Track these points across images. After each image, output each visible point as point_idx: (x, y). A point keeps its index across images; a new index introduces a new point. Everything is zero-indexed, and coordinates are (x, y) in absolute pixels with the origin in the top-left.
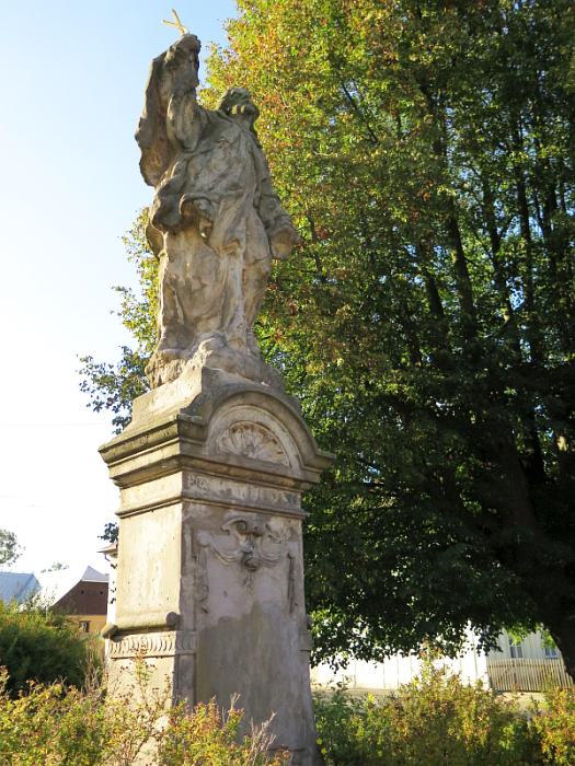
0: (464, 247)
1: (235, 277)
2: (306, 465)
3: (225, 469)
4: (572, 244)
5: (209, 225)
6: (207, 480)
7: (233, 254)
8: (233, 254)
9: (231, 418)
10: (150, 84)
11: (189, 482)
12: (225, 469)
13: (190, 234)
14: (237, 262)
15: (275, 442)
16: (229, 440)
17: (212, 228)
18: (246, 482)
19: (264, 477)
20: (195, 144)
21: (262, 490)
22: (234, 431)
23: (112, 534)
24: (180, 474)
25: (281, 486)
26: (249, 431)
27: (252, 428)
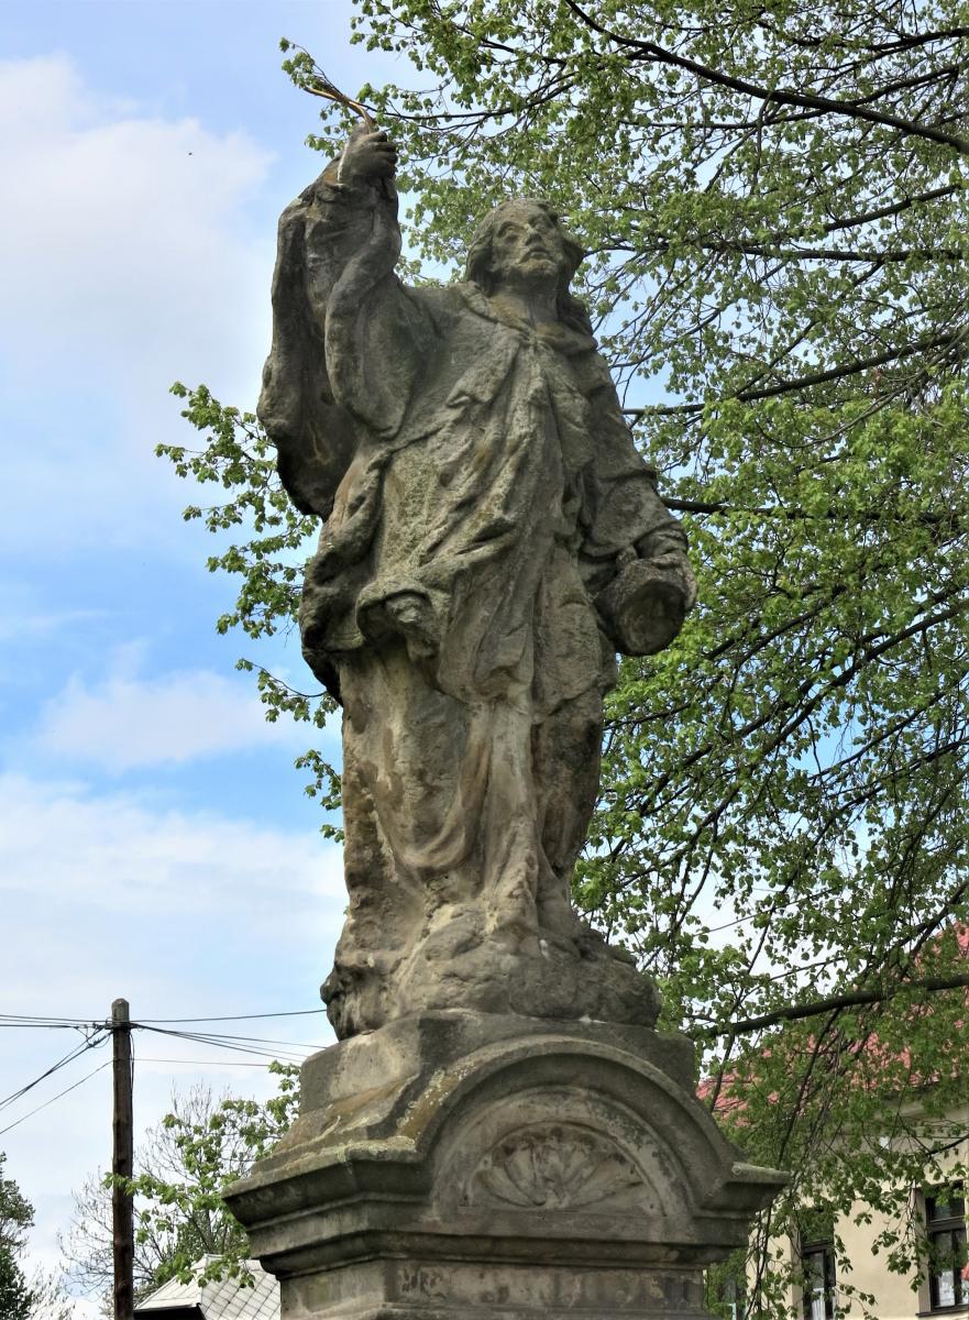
0: (825, 988)
1: (510, 760)
2: (703, 1208)
3: (487, 1245)
4: (967, 1003)
5: (427, 652)
6: (446, 1272)
7: (502, 698)
8: (502, 698)
9: (492, 1129)
10: (279, 283)
11: (402, 1282)
12: (487, 1245)
13: (395, 664)
14: (513, 717)
15: (622, 1160)
16: (499, 1174)
17: (433, 657)
18: (545, 1266)
19: (590, 1250)
20: (400, 412)
21: (591, 1277)
22: (509, 1151)
23: (249, 666)
24: (763, 101)
25: (638, 1265)
26: (553, 1143)
27: (558, 1134)
